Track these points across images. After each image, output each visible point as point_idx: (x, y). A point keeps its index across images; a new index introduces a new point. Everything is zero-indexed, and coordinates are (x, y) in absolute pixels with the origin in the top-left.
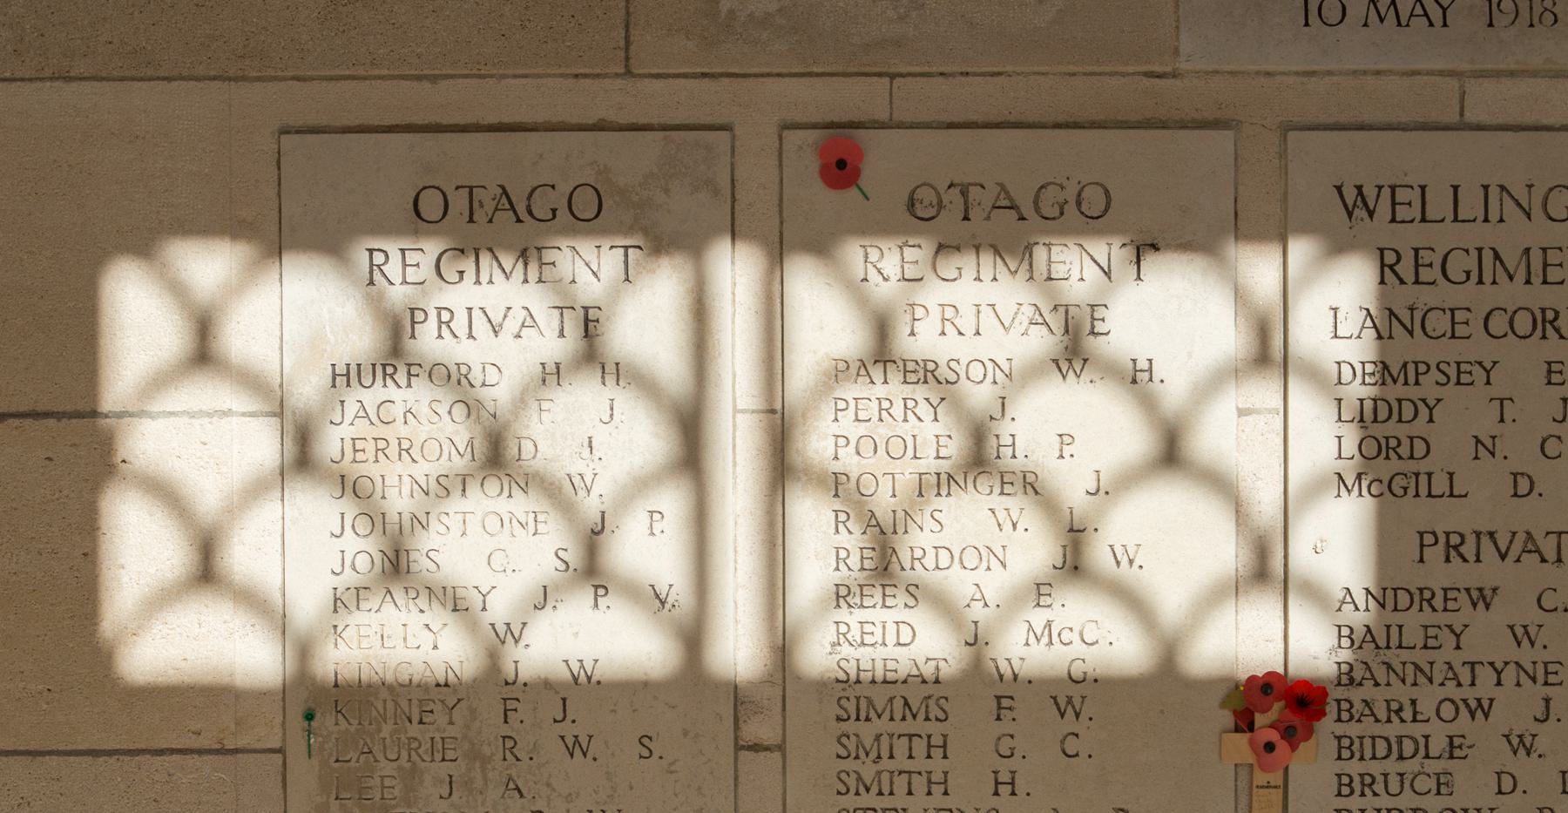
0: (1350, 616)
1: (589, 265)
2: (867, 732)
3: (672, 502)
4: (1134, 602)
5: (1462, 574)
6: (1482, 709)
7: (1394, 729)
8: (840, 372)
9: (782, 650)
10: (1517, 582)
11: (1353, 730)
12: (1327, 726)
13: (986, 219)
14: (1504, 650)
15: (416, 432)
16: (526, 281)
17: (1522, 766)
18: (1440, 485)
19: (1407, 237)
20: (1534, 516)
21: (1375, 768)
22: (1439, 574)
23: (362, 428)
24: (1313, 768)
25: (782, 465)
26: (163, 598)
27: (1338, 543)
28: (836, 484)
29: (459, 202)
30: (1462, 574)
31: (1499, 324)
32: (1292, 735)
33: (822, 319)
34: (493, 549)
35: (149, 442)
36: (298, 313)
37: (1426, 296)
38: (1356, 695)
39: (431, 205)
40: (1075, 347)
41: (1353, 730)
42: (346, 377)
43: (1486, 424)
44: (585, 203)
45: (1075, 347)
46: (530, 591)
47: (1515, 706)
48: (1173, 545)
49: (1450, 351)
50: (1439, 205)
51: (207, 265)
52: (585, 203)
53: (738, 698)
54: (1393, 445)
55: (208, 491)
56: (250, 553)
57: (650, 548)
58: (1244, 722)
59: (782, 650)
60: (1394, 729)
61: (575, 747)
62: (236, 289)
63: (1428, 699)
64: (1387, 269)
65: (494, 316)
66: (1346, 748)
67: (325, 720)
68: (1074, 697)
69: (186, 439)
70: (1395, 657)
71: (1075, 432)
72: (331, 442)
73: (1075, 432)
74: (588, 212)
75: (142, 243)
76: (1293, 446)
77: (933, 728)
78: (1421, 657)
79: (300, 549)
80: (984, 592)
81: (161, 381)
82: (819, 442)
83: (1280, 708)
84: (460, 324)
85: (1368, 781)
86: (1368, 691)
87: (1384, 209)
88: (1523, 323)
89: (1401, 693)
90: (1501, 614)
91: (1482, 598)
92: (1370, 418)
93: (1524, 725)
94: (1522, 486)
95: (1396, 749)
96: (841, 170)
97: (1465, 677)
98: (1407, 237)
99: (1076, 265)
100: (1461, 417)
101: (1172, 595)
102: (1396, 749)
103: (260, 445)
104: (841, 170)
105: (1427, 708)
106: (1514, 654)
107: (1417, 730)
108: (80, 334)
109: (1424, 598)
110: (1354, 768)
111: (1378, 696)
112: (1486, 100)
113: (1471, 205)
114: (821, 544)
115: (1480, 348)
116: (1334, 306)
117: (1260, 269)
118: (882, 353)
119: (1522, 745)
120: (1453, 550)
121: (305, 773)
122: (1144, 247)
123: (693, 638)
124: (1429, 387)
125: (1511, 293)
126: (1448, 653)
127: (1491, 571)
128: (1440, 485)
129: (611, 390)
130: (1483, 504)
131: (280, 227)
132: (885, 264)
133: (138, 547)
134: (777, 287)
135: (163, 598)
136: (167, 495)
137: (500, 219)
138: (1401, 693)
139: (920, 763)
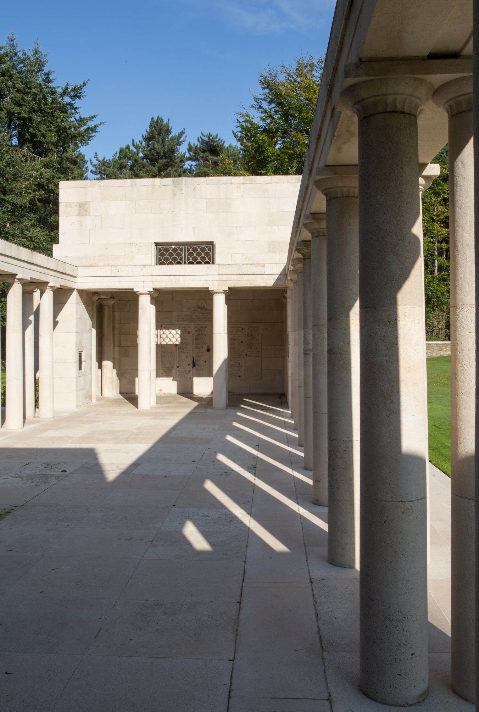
13: (167, 328)
25: (160, 337)
27: (179, 339)
33: (162, 332)
40: (170, 333)
45: (170, 333)
54: (181, 336)
71: (170, 336)
76: (178, 336)
83: (176, 345)
99: (170, 330)
114: (162, 340)
116: (179, 332)
134: (30, 330)
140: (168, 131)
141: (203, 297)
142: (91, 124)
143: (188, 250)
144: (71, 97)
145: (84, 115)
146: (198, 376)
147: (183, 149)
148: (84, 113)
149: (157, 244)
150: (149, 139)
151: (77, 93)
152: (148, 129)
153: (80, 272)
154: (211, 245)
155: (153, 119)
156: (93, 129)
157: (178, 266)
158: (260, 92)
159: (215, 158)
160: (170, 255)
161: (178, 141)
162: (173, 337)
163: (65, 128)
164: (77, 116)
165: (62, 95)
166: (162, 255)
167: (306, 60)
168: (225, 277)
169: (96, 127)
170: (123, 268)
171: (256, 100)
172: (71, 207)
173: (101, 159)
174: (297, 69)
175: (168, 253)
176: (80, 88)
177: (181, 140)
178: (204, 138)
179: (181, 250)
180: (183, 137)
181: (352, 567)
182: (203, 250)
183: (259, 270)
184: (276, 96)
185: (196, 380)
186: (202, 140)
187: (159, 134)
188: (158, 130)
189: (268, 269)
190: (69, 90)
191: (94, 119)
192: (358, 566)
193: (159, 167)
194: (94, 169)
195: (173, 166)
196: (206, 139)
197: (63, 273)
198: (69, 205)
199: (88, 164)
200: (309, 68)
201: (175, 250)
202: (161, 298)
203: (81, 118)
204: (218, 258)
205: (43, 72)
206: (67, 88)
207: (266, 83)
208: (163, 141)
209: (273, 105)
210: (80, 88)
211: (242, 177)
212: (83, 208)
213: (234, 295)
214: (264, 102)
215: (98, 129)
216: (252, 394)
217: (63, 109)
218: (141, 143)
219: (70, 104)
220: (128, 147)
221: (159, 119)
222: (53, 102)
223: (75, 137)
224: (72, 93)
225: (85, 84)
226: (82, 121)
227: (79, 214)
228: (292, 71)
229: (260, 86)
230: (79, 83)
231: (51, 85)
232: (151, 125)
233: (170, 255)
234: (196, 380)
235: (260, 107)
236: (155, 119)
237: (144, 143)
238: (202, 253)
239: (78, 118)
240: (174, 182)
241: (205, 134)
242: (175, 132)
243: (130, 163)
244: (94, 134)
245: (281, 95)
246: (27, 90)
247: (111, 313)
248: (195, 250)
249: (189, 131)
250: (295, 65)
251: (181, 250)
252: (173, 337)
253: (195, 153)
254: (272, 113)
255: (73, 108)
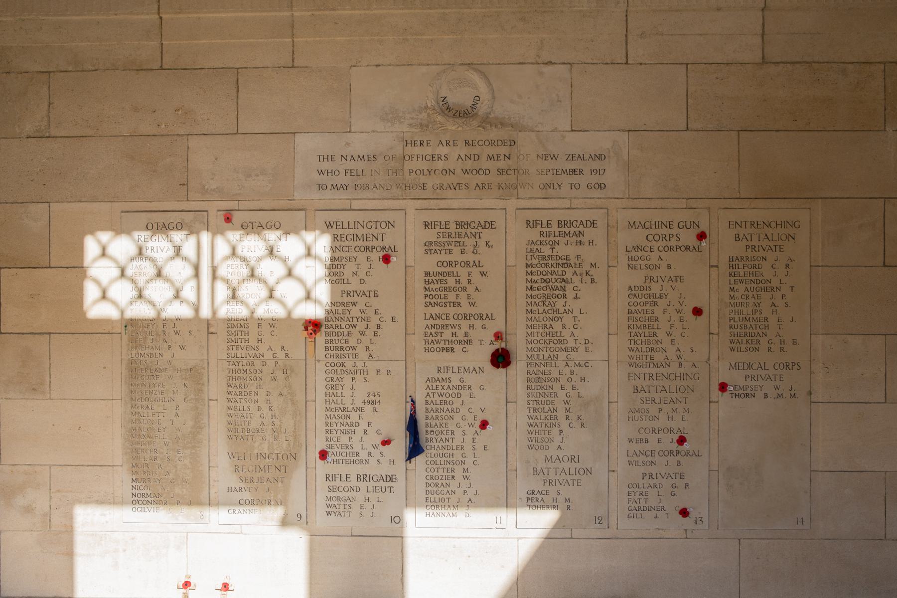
0: (328, 307)
1: (178, 236)
2: (233, 330)
3: (193, 283)
4: (282, 303)
5: (350, 299)
6: (354, 326)
7: (337, 330)
8: (226, 258)
9: (214, 313)
10: (362, 301)
11: (329, 330)
12: (323, 329)
14: (359, 314)
15: (143, 270)
16: (630, 441)
17: (362, 338)
18: (346, 281)
19: (339, 232)
20: (365, 288)
21: (333, 338)
22: (345, 299)
23: (136, 270)
24: (321, 338)
26: (95, 302)
27: (323, 292)
28: (227, 281)
29: (155, 226)
30: (350, 299)
31: (357, 249)
32: (315, 332)
33: (222, 248)
34: (159, 292)
35: (93, 272)
36: (122, 246)
37: (343, 244)
38: (329, 323)
39: (150, 226)
40: (271, 252)
41: (329, 330)
42: (132, 259)
43: (355, 269)
44: (179, 226)
46: (164, 302)
47: (361, 326)
48: (290, 291)
49: (348, 255)
50: (345, 226)
51: (105, 236)
52: (179, 226)
53: (208, 323)
54: (335, 271)
55: (105, 281)
56: (112, 293)
57: (188, 292)
58: (306, 329)
59: (214, 313)
60: (337, 330)
61: (177, 333)
62: (110, 241)
63: (344, 324)
64: (335, 238)
65: (160, 246)
66: (327, 334)
67: (129, 328)
68: (273, 323)
69: (100, 271)
70: (337, 316)
71: (271, 269)
72: (129, 272)
73: (271, 269)
74: (179, 227)
75: (92, 232)
76: (314, 272)
77: (246, 330)
78: (342, 316)
79: (122, 292)
80: (254, 302)
81: (95, 260)
82: (222, 271)
83: (314, 326)
84: (155, 250)
85: (331, 341)
86: (331, 323)
87: (334, 226)
88: (362, 249)
89: (338, 323)
90: (358, 307)
91: (354, 304)
92: (330, 268)
93: (363, 329)
94: (362, 281)
95: (337, 334)
96: (228, 220)
97: (749, 238)
98: (339, 232)
99: (272, 236)
100: (350, 267)
101: (290, 302)
102: (337, 334)
103: (116, 272)
104: (228, 220)
105: (343, 326)
106: (360, 315)
107: (341, 331)
108: (80, 250)
109: (342, 304)
110: (329, 338)
111: (334, 324)
112: (356, 204)
113: (352, 226)
114: (222, 292)
115: (354, 254)
116: (322, 244)
117: (309, 237)
118: (234, 253)
119: (362, 334)
120: (348, 294)
121: (125, 337)
122: (287, 233)
123: (197, 310)
124: (343, 262)
125: (360, 243)
126: (347, 315)
127: (356, 299)
128: (346, 281)
129: (184, 263)
130: (354, 285)
131: (119, 230)
132: (234, 236)
133: (91, 292)
135: (95, 302)
136: (97, 282)
137: (162, 228)
138: (338, 323)
139: (243, 337)
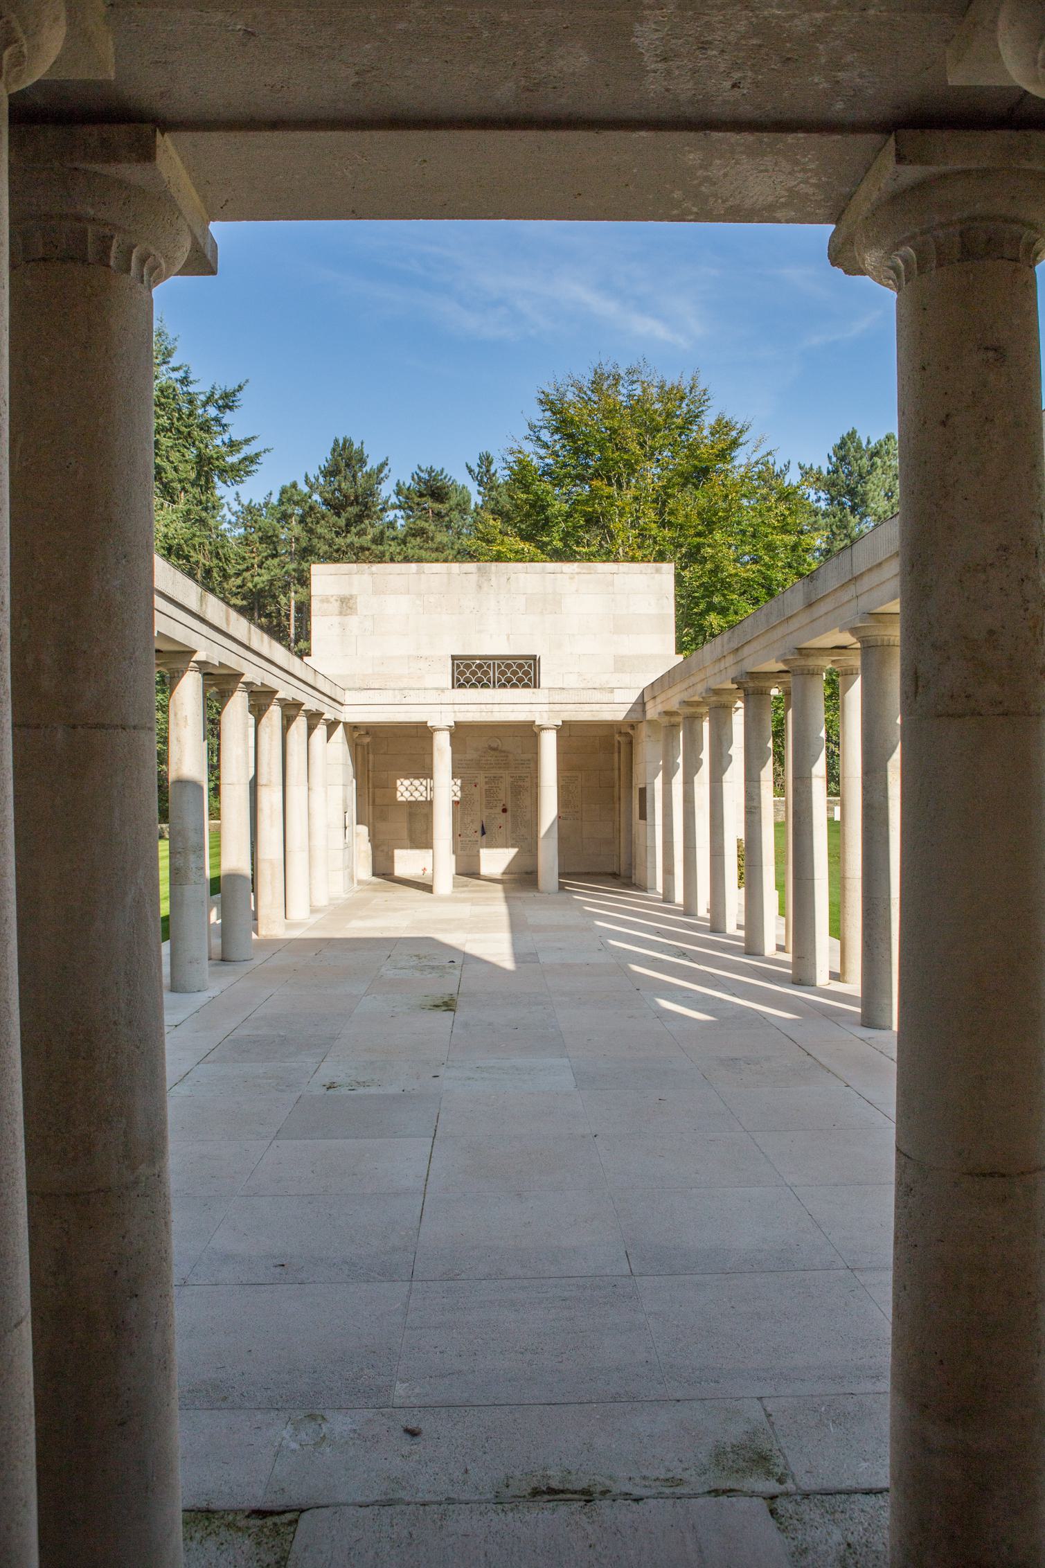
76: (401, 789)
140: (362, 462)
141: (529, 733)
142: (247, 451)
143: (499, 666)
144: (219, 408)
145: (238, 437)
146: (490, 845)
147: (386, 491)
148: (236, 433)
149: (454, 658)
150: (331, 472)
151: (227, 402)
152: (330, 456)
153: (348, 698)
154: (534, 660)
155: (336, 441)
156: (252, 459)
157: (473, 690)
158: (538, 415)
159: (437, 506)
160: (474, 673)
161: (377, 475)
162: (407, 790)
163: (212, 457)
164: (226, 438)
165: (204, 405)
166: (462, 673)
167: (607, 369)
168: (557, 707)
169: (257, 455)
170: (412, 692)
171: (532, 427)
172: (328, 601)
173: (246, 503)
174: (593, 382)
175: (470, 672)
176: (234, 394)
177: (382, 475)
178: (422, 475)
179: (489, 666)
180: (386, 471)
181: (890, 1028)
182: (520, 666)
183: (605, 697)
184: (564, 426)
185: (484, 853)
186: (419, 477)
187: (348, 465)
188: (345, 459)
189: (619, 696)
190: (216, 397)
191: (253, 443)
192: (895, 1027)
193: (348, 520)
194: (233, 519)
195: (368, 516)
196: (424, 476)
197: (334, 700)
198: (326, 600)
199: (225, 511)
200: (611, 381)
201: (480, 666)
202: (460, 732)
203: (231, 441)
204: (544, 680)
205: (171, 366)
206: (212, 394)
207: (547, 403)
208: (354, 476)
209: (557, 437)
210: (234, 394)
211: (576, 564)
212: (346, 604)
213: (569, 732)
214: (545, 431)
215: (261, 459)
216: (588, 874)
217: (205, 427)
218: (317, 479)
219: (217, 420)
220: (294, 486)
221: (347, 443)
222: (190, 415)
223: (226, 471)
224: (220, 402)
225: (240, 388)
226: (233, 446)
227: (341, 614)
228: (586, 384)
229: (539, 408)
230: (230, 389)
231: (191, 389)
232: (334, 450)
233: (474, 673)
234: (484, 853)
235: (539, 439)
236: (341, 442)
237: (321, 480)
238: (521, 671)
239: (227, 441)
240: (479, 569)
241: (424, 468)
242: (372, 464)
243: (298, 511)
244: (254, 467)
245: (572, 422)
246: (163, 400)
247: (383, 754)
248: (509, 666)
249: (397, 463)
250: (591, 376)
251: (489, 666)
252: (407, 790)
253: (407, 498)
254: (557, 447)
255: (221, 425)
